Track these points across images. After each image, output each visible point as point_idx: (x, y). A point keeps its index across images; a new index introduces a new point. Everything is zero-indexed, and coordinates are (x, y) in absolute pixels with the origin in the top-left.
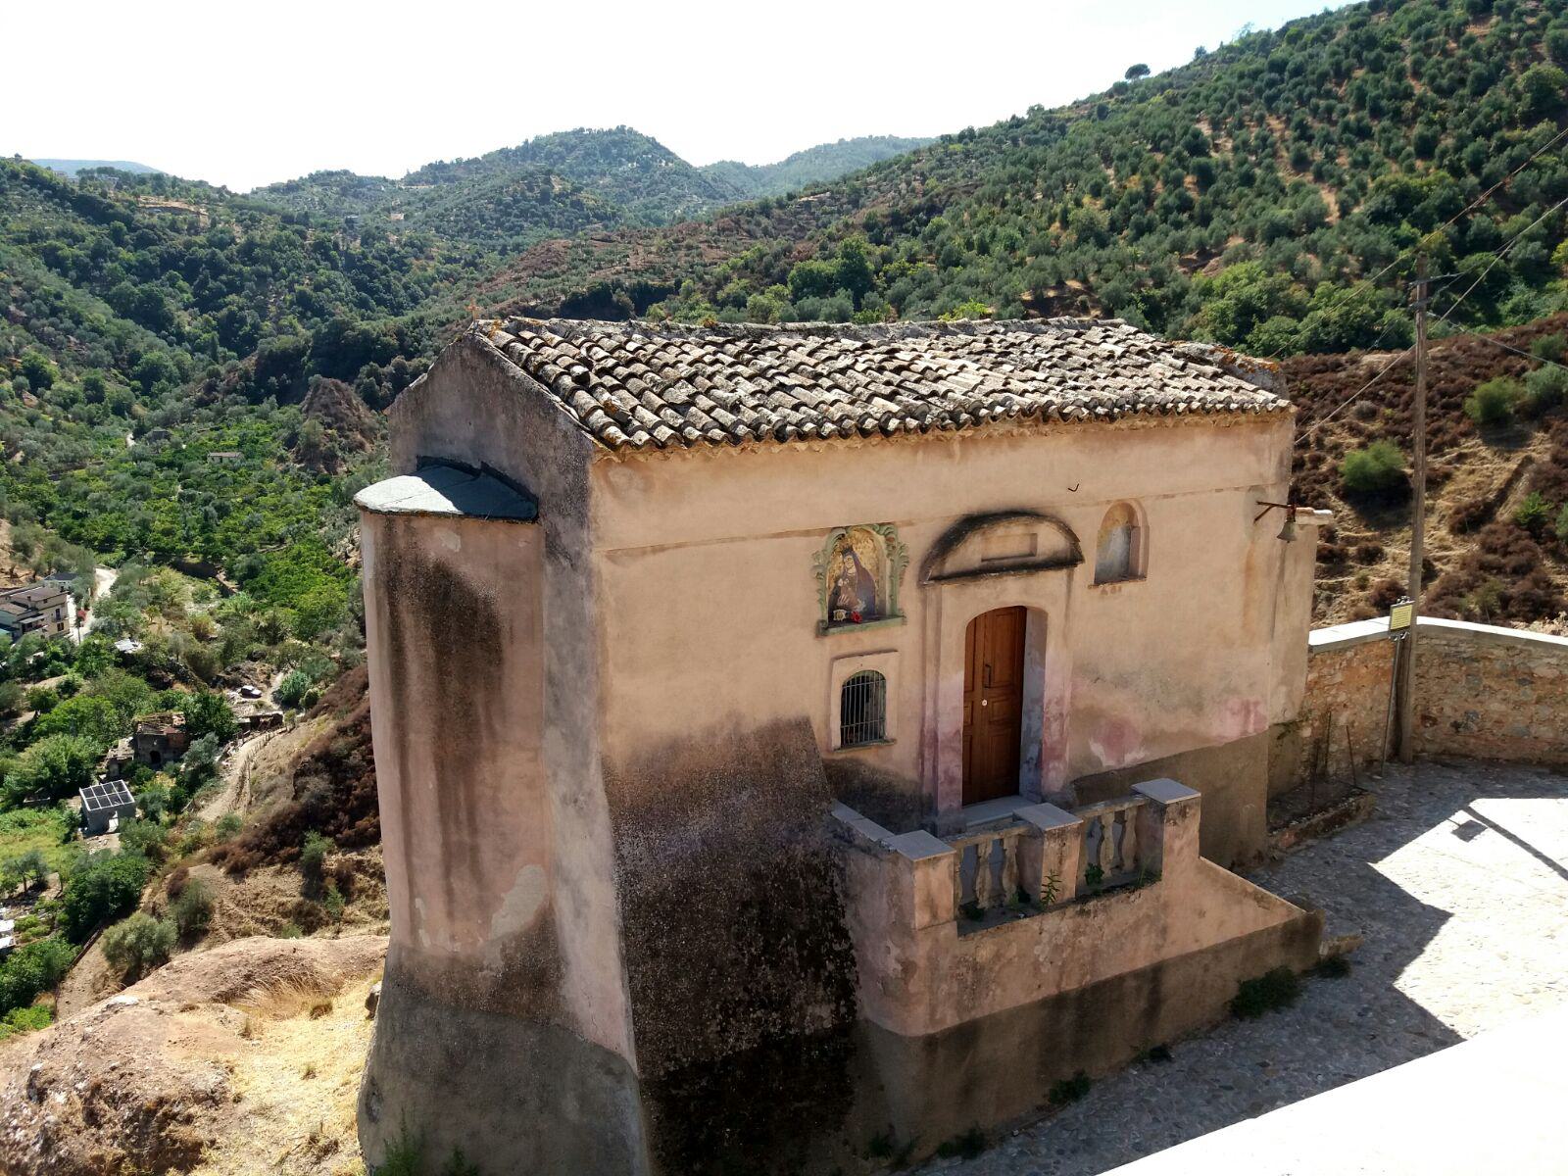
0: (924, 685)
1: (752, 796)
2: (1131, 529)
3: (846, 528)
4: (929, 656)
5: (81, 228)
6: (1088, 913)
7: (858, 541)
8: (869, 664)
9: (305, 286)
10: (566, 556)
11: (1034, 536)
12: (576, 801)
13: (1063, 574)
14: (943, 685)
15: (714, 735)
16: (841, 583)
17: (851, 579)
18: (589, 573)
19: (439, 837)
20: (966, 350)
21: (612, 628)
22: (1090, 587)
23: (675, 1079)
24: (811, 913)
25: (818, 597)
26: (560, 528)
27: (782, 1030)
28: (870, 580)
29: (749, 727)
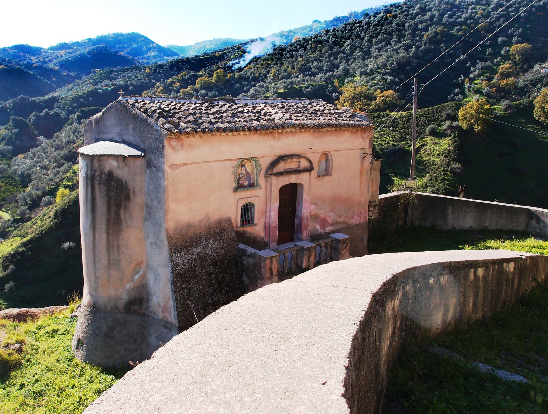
0: (266, 207)
1: (213, 241)
2: (327, 160)
3: (243, 159)
4: (268, 199)
7: (246, 163)
8: (250, 200)
10: (155, 167)
11: (299, 162)
12: (156, 243)
13: (308, 173)
14: (272, 207)
15: (201, 222)
17: (244, 175)
18: (163, 172)
19: (107, 258)
20: (277, 107)
21: (170, 189)
22: (316, 178)
25: (234, 180)
26: (153, 158)
28: (250, 175)
29: (212, 220)
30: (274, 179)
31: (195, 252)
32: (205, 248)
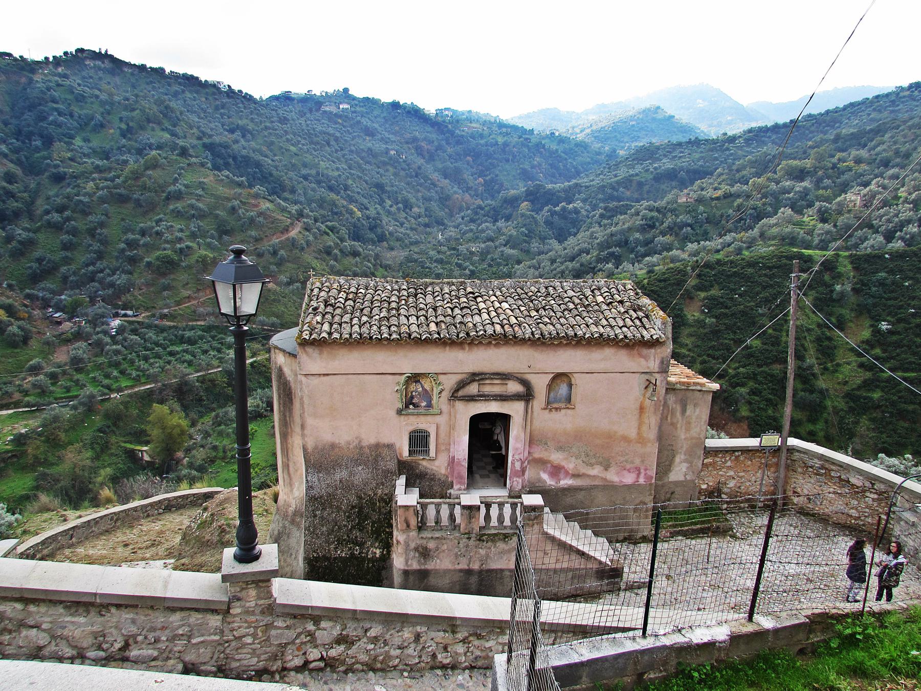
5: (434, 136)
6: (483, 541)
9: (527, 166)
16: (414, 394)
23: (317, 559)
24: (380, 515)
27: (359, 554)
30: (459, 405)
31: (337, 477)
32: (351, 474)
